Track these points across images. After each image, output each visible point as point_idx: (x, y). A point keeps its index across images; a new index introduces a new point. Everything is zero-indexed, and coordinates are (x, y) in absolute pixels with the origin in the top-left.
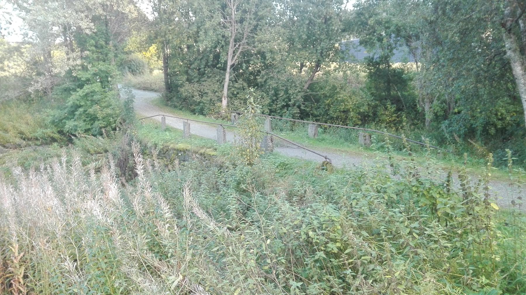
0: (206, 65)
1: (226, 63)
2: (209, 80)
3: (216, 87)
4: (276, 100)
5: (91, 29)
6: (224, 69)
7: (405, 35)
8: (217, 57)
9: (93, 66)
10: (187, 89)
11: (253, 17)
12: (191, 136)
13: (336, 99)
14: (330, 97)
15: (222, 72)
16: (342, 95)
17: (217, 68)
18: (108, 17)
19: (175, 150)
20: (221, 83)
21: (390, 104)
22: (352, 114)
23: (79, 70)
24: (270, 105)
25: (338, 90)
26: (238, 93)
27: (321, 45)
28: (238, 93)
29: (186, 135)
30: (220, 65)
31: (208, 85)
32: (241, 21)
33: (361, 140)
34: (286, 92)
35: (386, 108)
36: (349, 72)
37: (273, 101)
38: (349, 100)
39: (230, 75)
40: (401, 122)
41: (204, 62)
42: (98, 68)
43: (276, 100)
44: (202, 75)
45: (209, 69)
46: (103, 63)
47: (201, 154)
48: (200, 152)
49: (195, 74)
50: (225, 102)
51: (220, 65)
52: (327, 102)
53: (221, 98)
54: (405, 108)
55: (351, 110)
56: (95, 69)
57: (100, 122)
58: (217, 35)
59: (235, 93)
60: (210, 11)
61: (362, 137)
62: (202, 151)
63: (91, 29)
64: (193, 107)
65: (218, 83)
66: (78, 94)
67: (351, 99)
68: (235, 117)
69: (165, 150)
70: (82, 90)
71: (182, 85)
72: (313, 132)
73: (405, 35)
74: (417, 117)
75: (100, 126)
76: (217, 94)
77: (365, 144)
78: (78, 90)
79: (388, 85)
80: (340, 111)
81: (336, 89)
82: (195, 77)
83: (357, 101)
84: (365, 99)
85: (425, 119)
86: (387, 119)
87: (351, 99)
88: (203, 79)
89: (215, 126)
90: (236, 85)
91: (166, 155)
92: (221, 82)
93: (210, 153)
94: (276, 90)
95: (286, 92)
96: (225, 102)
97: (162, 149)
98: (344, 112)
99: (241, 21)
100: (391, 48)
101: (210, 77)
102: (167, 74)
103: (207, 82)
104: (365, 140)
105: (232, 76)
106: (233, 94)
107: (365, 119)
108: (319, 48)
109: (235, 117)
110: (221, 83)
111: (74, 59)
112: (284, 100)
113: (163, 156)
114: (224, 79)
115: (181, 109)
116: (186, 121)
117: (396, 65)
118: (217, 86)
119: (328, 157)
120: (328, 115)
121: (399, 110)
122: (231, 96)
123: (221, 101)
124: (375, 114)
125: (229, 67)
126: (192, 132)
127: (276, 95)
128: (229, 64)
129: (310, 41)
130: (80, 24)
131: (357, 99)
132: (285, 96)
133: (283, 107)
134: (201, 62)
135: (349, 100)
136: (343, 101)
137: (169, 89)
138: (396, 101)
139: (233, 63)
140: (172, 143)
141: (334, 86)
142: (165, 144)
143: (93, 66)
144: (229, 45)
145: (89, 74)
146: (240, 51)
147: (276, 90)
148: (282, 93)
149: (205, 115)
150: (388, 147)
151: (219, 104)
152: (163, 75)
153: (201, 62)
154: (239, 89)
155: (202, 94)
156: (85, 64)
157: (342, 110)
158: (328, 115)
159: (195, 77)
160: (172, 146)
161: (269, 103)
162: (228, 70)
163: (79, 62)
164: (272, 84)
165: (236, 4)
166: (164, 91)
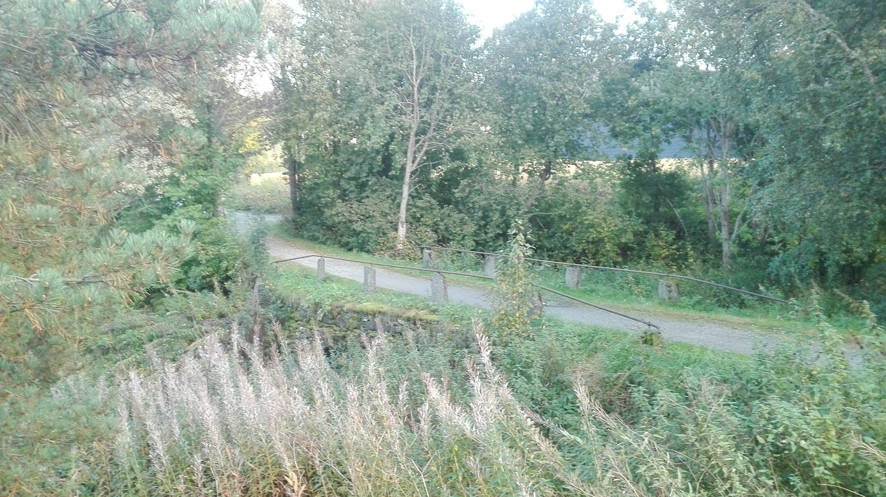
0: (370, 172)
1: (403, 169)
2: (374, 196)
3: (386, 206)
4: (485, 225)
5: (189, 118)
6: (400, 178)
7: (685, 122)
8: (387, 160)
9: (190, 177)
10: (339, 212)
11: (446, 96)
12: (376, 290)
13: (580, 223)
14: (570, 219)
15: (395, 182)
16: (591, 217)
17: (387, 177)
18: (216, 100)
19: (354, 312)
20: (394, 200)
21: (663, 230)
22: (608, 247)
23: (166, 184)
24: (476, 234)
25: (584, 208)
26: (422, 216)
27: (555, 139)
28: (422, 216)
29: (368, 288)
30: (393, 172)
31: (373, 204)
32: (428, 104)
33: (662, 291)
34: (503, 213)
35: (657, 235)
36: (599, 180)
37: (480, 227)
38: (604, 225)
39: (410, 188)
40: (685, 257)
41: (366, 168)
42: (197, 181)
43: (485, 225)
44: (362, 186)
45: (374, 179)
46: (204, 173)
47: (408, 320)
48: (404, 316)
49: (351, 186)
50: (402, 231)
51: (393, 172)
52: (565, 227)
53: (397, 225)
54: (687, 234)
55: (606, 240)
56: (193, 182)
57: (202, 268)
58: (392, 126)
59: (418, 215)
60: (381, 89)
61: (665, 288)
62: (412, 313)
63: (189, 118)
64: (345, 239)
65: (390, 201)
66: (165, 223)
67: (606, 222)
68: (430, 255)
69: (335, 313)
70: (171, 217)
71: (331, 205)
72: (576, 280)
73: (685, 122)
74: (709, 248)
75: (204, 274)
76: (389, 218)
77: (670, 298)
78: (165, 216)
79: (655, 198)
80: (588, 242)
81: (580, 207)
82: (351, 192)
83: (616, 226)
84: (628, 223)
85: (721, 252)
86: (665, 252)
87: (606, 222)
88: (364, 195)
89: (397, 272)
90: (420, 203)
91: (337, 321)
92: (395, 199)
93: (425, 317)
94: (486, 212)
95: (503, 213)
96: (402, 231)
97: (330, 312)
98: (593, 243)
99: (428, 104)
100: (656, 141)
101: (376, 190)
102: (296, 185)
103: (370, 199)
104: (670, 291)
105: (413, 189)
106: (414, 217)
107: (626, 253)
108: (552, 144)
109: (430, 255)
110: (394, 200)
111: (160, 168)
112: (498, 226)
113: (330, 322)
114: (401, 194)
115: (324, 243)
116: (369, 266)
117: (666, 165)
118: (387, 205)
119: (652, 323)
120: (566, 248)
121: (679, 237)
122: (411, 220)
123: (396, 230)
124: (641, 244)
125: (408, 174)
126: (378, 284)
127: (485, 217)
128: (409, 169)
129: (537, 136)
130: (173, 112)
131: (615, 223)
132: (500, 220)
133: (498, 236)
134: (361, 168)
135: (604, 225)
136: (592, 226)
137: (299, 209)
138: (672, 223)
139: (414, 168)
140: (348, 302)
141: (577, 202)
142: (336, 304)
143: (190, 177)
144: (408, 140)
145: (184, 191)
146: (424, 149)
147: (486, 212)
148: (496, 217)
149: (368, 252)
150: (817, 316)
151: (392, 234)
152: (286, 188)
153: (361, 168)
154: (423, 209)
155: (368, 217)
156: (176, 174)
157: (590, 239)
158: (566, 248)
159: (351, 192)
160: (348, 306)
161: (475, 232)
162: (407, 179)
163: (167, 171)
164: (480, 201)
165: (420, 78)
166: (290, 215)
